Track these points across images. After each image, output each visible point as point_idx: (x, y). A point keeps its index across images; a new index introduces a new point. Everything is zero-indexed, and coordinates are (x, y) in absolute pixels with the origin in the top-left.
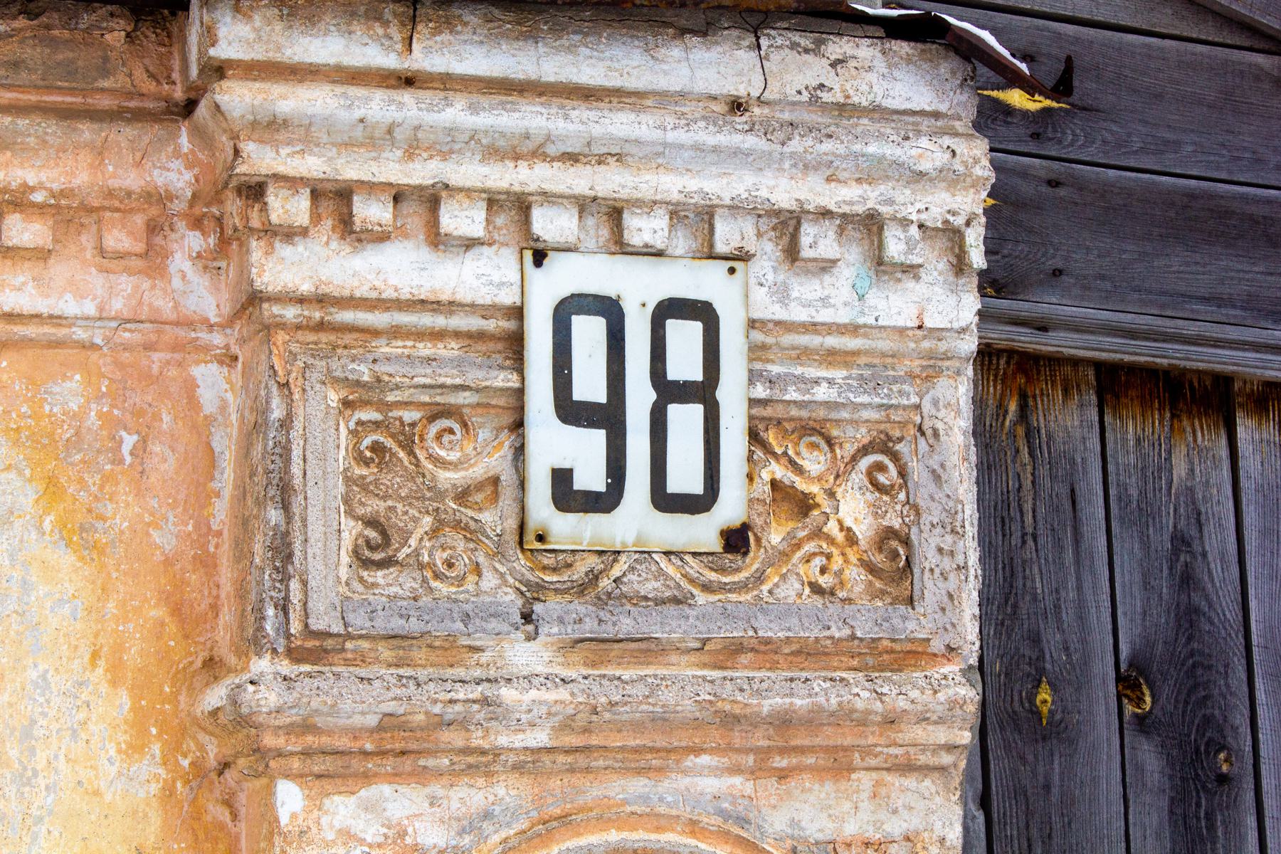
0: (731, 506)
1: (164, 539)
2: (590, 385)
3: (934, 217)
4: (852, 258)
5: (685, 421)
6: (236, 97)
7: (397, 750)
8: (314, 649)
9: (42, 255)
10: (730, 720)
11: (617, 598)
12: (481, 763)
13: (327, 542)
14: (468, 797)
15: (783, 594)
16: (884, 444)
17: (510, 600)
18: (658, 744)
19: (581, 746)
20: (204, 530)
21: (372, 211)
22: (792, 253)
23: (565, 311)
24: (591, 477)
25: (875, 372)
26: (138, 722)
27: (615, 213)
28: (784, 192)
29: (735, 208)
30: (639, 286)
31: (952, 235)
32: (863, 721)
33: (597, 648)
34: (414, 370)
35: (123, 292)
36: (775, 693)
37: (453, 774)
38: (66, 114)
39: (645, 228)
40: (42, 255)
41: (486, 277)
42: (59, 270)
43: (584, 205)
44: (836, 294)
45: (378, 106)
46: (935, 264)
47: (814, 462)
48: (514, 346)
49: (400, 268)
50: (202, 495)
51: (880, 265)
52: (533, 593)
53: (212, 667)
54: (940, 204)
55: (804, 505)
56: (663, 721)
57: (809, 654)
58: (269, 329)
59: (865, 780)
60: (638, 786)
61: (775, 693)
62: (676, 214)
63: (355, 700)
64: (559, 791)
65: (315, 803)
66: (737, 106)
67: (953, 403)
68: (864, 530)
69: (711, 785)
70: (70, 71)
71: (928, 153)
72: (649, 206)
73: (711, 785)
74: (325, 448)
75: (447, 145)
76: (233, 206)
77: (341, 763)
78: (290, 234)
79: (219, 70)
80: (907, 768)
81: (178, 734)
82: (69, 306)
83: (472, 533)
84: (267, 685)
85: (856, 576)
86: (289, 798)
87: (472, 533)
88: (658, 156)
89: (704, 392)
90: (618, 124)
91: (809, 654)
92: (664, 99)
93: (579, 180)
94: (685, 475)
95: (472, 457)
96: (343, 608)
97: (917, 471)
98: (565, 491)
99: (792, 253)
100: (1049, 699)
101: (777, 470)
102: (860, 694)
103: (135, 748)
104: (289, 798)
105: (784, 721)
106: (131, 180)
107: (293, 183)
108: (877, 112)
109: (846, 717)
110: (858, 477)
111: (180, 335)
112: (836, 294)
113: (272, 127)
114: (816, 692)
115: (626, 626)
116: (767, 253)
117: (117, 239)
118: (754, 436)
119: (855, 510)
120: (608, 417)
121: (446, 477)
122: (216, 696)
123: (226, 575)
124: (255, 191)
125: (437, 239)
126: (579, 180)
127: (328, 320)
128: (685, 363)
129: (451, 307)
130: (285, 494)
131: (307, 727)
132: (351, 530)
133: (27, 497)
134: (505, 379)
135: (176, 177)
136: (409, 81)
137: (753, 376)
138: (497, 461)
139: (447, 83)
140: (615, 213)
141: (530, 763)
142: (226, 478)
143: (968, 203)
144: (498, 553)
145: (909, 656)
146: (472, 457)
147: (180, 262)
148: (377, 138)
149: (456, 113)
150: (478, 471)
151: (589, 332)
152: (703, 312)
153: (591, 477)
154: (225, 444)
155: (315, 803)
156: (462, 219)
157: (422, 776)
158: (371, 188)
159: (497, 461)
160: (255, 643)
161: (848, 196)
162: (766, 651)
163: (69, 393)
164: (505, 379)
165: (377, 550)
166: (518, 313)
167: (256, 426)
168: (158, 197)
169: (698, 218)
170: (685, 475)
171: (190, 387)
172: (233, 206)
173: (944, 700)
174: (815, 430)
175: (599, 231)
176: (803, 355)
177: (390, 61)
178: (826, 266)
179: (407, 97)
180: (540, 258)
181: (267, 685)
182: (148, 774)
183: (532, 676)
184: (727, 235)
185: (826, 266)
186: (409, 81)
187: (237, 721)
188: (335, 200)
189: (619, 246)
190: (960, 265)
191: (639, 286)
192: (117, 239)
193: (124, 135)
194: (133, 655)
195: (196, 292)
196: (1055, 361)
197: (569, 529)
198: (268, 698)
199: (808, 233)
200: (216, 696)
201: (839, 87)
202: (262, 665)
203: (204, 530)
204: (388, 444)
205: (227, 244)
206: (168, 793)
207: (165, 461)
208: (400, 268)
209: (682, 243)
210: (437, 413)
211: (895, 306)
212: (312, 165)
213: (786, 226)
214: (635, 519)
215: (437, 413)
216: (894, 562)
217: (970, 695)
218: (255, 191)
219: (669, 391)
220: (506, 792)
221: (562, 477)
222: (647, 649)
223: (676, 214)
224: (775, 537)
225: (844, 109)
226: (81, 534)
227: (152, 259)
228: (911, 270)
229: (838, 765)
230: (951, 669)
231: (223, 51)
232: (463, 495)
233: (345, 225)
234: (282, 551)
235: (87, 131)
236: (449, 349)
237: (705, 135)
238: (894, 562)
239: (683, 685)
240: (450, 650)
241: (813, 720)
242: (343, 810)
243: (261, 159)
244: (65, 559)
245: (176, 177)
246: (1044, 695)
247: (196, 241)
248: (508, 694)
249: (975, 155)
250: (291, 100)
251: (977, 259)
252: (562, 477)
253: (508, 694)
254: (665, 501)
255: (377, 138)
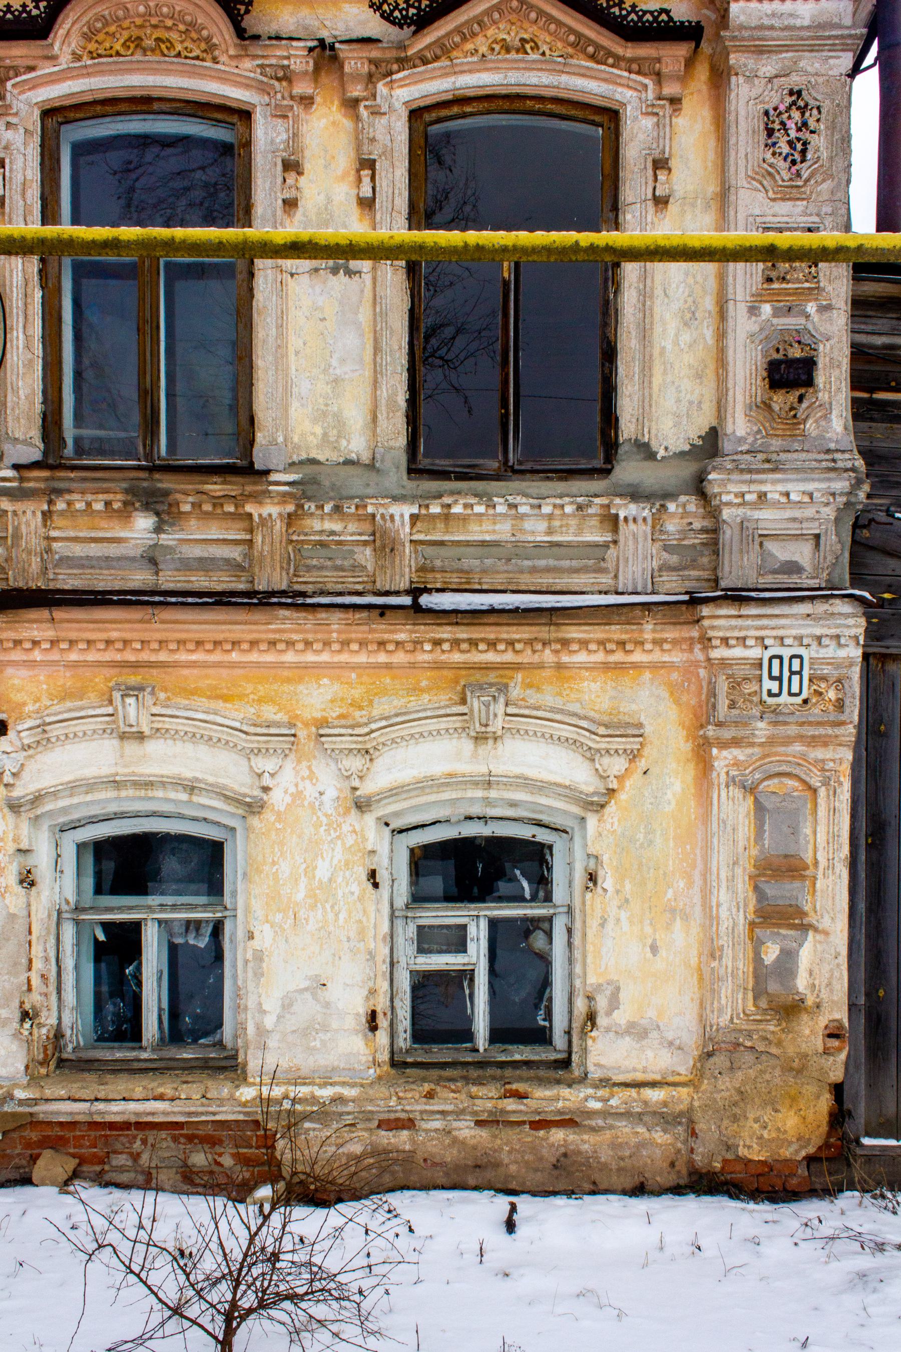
0: (805, 695)
1: (693, 702)
2: (776, 672)
3: (852, 634)
4: (833, 644)
5: (796, 679)
6: (706, 623)
7: (736, 742)
8: (720, 724)
9: (670, 650)
10: (802, 736)
11: (781, 713)
12: (752, 745)
13: (723, 704)
14: (749, 751)
15: (816, 711)
16: (839, 681)
17: (758, 714)
18: (788, 741)
19: (771, 741)
20: (700, 700)
21: (732, 642)
22: (820, 644)
23: (771, 659)
24: (775, 690)
25: (838, 666)
26: (688, 737)
27: (782, 639)
28: (818, 631)
29: (807, 636)
30: (786, 653)
31: (856, 638)
32: (830, 736)
33: (775, 723)
34: (741, 672)
35: (685, 656)
36: (811, 731)
37: (746, 747)
38: (674, 624)
39: (787, 641)
40: (670, 650)
41: (755, 653)
42: (673, 653)
43: (775, 638)
44: (830, 651)
45: (733, 622)
46: (852, 643)
47: (823, 685)
48: (760, 665)
49: (738, 652)
50: (700, 694)
51: (840, 645)
52: (763, 713)
53: (702, 726)
54: (853, 632)
55: (821, 694)
56: (788, 737)
57: (819, 724)
58: (712, 665)
59: (831, 747)
60: (783, 749)
61: (811, 731)
62: (795, 638)
63: (727, 734)
64: (767, 750)
65: (720, 752)
66: (808, 615)
67: (856, 673)
68: (833, 699)
69: (798, 748)
70: (675, 616)
71: (851, 621)
72: (788, 637)
73: (798, 748)
74: (723, 686)
75: (748, 628)
76: (706, 641)
77: (724, 745)
78: (716, 647)
79: (703, 617)
80: (840, 745)
81: (695, 738)
82: (675, 659)
83: (751, 702)
84: (711, 731)
85: (831, 708)
86: (715, 751)
87: (751, 702)
88: (791, 627)
89: (800, 673)
90: (783, 622)
91: (819, 724)
92: (793, 615)
93: (775, 633)
94: (795, 689)
95: (752, 687)
96: (726, 716)
97: (846, 686)
98: (770, 694)
99: (820, 644)
100: (356, 894)
101: (815, 687)
102: (830, 731)
103: (687, 741)
104: (715, 751)
105: (813, 737)
106: (687, 635)
107: (717, 638)
108: (840, 614)
109: (827, 736)
110: (833, 687)
111: (696, 664)
112: (830, 651)
113: (713, 628)
114: (821, 731)
115: (781, 719)
116: (814, 645)
117: (684, 647)
118: (810, 680)
119: (832, 694)
120: (780, 679)
121: (746, 691)
122: (701, 733)
123: (704, 708)
124: (710, 639)
125: (745, 646)
126: (775, 633)
127: (724, 663)
128: (796, 666)
129: (748, 659)
130: (715, 696)
131: (718, 739)
132: (727, 702)
133: (667, 695)
134: (758, 672)
135: (695, 634)
136: (740, 616)
137: (810, 669)
138: (757, 688)
139: (748, 616)
140: (782, 639)
141: (761, 745)
142: (705, 691)
143: (860, 631)
144: (756, 705)
145: (842, 723)
146: (752, 687)
147: (696, 650)
148: (733, 628)
149: (749, 622)
150: (752, 690)
151: (776, 663)
152: (800, 657)
153: (775, 690)
154: (705, 684)
155: (720, 752)
156: (750, 642)
157: (740, 747)
158: (732, 638)
159: (757, 688)
160: (709, 723)
161: (833, 631)
162: (810, 723)
163: (675, 676)
164: (758, 672)
165: (732, 705)
166: (761, 659)
167: (710, 683)
168: (692, 638)
169: (799, 639)
170: (795, 689)
171: (698, 674)
172: (706, 641)
173: (849, 732)
174: (824, 678)
175: (778, 642)
176: (822, 664)
177: (736, 613)
178: (827, 646)
179: (739, 620)
180: (766, 648)
181: (711, 731)
182: (689, 746)
183: (762, 729)
184: (805, 641)
185: (827, 646)
186: (740, 616)
187: (705, 737)
188: (725, 641)
189: (783, 645)
190: (858, 644)
191: (786, 653)
192: (684, 647)
193: (685, 627)
194: (687, 723)
195: (698, 654)
196: (891, 655)
197: (771, 701)
198: (710, 733)
199: (823, 640)
200: (701, 733)
201: (831, 609)
202: (710, 727)
203: (700, 700)
204: (735, 685)
205: (705, 648)
206: (693, 750)
207: (693, 688)
208: (738, 652)
209: (796, 643)
210: (744, 679)
211: (842, 653)
212: (721, 634)
213: (819, 639)
214: (784, 698)
215: (744, 679)
216: (840, 705)
217: (854, 731)
218: (710, 639)
219: (792, 673)
220: (756, 750)
221: (769, 691)
222: (786, 723)
223: (795, 638)
224: (814, 701)
225: (833, 614)
226: (677, 702)
227: (691, 650)
228: (847, 646)
229: (825, 745)
230: (851, 726)
231: (704, 614)
232: (749, 695)
233: (727, 645)
234: (714, 706)
235: (678, 627)
236: (748, 667)
237: (801, 622)
238: (840, 705)
239: (793, 730)
240: (746, 724)
241: (820, 736)
242: (725, 753)
243: (711, 633)
244: (674, 706)
245: (695, 634)
246: (882, 727)
247: (699, 646)
248: (757, 732)
249: (863, 621)
250: (716, 622)
251: (862, 642)
252: (769, 691)
253: (757, 732)
254: (790, 694)
255: (733, 628)
